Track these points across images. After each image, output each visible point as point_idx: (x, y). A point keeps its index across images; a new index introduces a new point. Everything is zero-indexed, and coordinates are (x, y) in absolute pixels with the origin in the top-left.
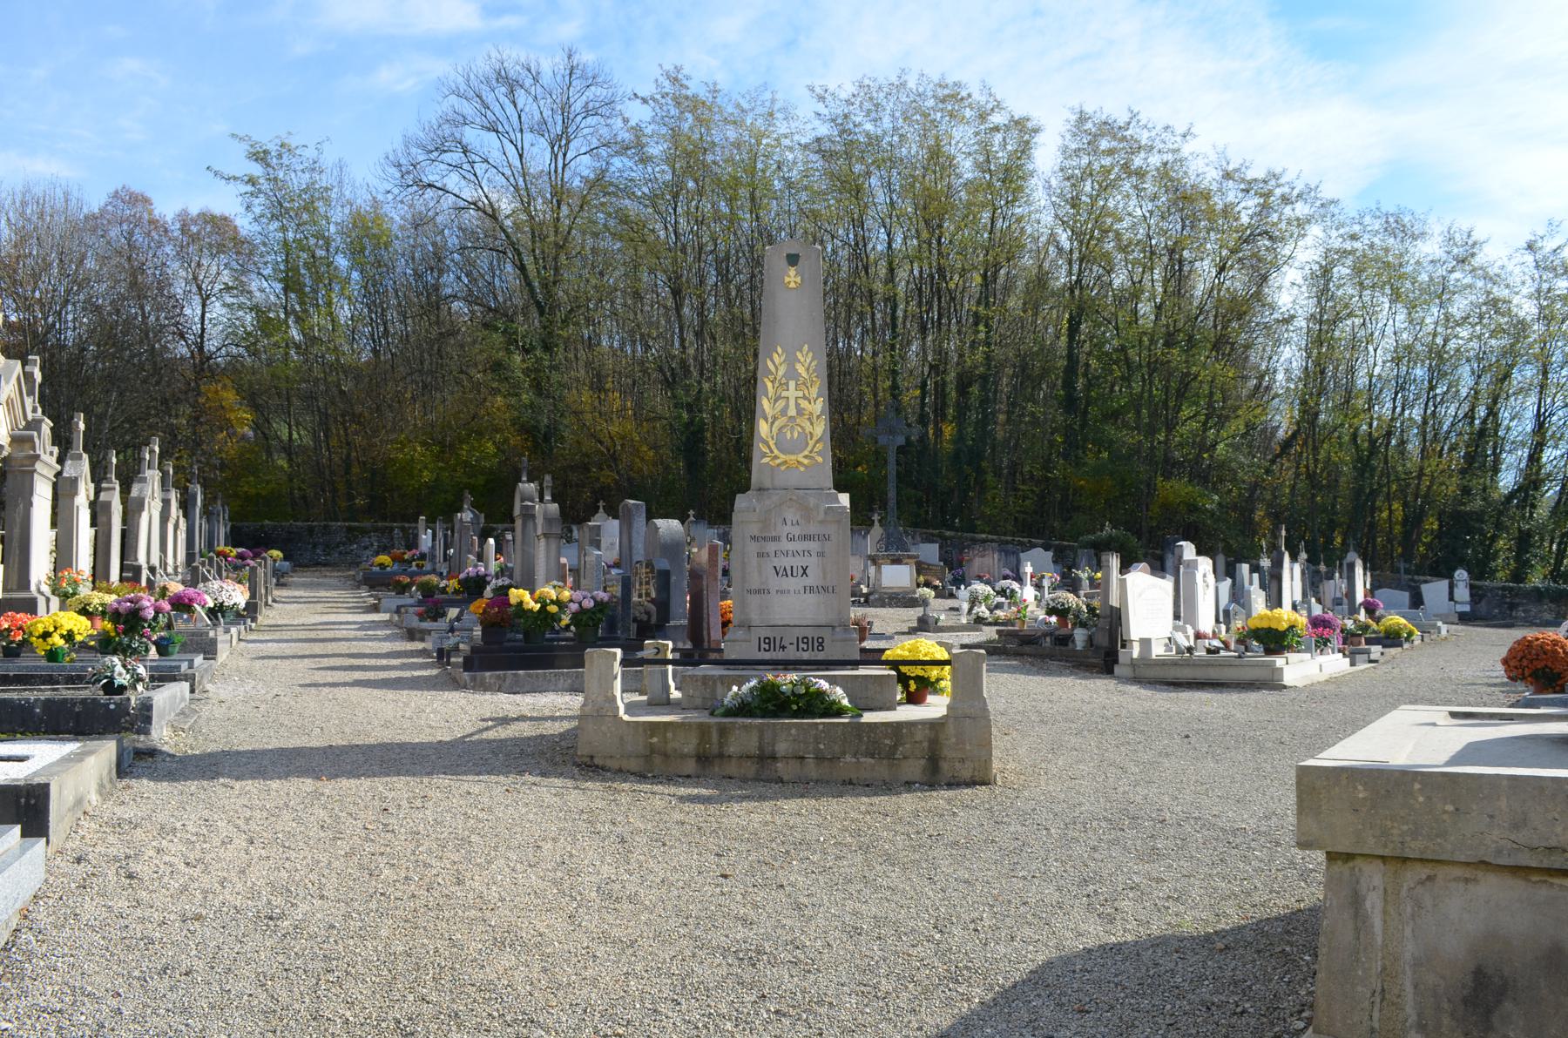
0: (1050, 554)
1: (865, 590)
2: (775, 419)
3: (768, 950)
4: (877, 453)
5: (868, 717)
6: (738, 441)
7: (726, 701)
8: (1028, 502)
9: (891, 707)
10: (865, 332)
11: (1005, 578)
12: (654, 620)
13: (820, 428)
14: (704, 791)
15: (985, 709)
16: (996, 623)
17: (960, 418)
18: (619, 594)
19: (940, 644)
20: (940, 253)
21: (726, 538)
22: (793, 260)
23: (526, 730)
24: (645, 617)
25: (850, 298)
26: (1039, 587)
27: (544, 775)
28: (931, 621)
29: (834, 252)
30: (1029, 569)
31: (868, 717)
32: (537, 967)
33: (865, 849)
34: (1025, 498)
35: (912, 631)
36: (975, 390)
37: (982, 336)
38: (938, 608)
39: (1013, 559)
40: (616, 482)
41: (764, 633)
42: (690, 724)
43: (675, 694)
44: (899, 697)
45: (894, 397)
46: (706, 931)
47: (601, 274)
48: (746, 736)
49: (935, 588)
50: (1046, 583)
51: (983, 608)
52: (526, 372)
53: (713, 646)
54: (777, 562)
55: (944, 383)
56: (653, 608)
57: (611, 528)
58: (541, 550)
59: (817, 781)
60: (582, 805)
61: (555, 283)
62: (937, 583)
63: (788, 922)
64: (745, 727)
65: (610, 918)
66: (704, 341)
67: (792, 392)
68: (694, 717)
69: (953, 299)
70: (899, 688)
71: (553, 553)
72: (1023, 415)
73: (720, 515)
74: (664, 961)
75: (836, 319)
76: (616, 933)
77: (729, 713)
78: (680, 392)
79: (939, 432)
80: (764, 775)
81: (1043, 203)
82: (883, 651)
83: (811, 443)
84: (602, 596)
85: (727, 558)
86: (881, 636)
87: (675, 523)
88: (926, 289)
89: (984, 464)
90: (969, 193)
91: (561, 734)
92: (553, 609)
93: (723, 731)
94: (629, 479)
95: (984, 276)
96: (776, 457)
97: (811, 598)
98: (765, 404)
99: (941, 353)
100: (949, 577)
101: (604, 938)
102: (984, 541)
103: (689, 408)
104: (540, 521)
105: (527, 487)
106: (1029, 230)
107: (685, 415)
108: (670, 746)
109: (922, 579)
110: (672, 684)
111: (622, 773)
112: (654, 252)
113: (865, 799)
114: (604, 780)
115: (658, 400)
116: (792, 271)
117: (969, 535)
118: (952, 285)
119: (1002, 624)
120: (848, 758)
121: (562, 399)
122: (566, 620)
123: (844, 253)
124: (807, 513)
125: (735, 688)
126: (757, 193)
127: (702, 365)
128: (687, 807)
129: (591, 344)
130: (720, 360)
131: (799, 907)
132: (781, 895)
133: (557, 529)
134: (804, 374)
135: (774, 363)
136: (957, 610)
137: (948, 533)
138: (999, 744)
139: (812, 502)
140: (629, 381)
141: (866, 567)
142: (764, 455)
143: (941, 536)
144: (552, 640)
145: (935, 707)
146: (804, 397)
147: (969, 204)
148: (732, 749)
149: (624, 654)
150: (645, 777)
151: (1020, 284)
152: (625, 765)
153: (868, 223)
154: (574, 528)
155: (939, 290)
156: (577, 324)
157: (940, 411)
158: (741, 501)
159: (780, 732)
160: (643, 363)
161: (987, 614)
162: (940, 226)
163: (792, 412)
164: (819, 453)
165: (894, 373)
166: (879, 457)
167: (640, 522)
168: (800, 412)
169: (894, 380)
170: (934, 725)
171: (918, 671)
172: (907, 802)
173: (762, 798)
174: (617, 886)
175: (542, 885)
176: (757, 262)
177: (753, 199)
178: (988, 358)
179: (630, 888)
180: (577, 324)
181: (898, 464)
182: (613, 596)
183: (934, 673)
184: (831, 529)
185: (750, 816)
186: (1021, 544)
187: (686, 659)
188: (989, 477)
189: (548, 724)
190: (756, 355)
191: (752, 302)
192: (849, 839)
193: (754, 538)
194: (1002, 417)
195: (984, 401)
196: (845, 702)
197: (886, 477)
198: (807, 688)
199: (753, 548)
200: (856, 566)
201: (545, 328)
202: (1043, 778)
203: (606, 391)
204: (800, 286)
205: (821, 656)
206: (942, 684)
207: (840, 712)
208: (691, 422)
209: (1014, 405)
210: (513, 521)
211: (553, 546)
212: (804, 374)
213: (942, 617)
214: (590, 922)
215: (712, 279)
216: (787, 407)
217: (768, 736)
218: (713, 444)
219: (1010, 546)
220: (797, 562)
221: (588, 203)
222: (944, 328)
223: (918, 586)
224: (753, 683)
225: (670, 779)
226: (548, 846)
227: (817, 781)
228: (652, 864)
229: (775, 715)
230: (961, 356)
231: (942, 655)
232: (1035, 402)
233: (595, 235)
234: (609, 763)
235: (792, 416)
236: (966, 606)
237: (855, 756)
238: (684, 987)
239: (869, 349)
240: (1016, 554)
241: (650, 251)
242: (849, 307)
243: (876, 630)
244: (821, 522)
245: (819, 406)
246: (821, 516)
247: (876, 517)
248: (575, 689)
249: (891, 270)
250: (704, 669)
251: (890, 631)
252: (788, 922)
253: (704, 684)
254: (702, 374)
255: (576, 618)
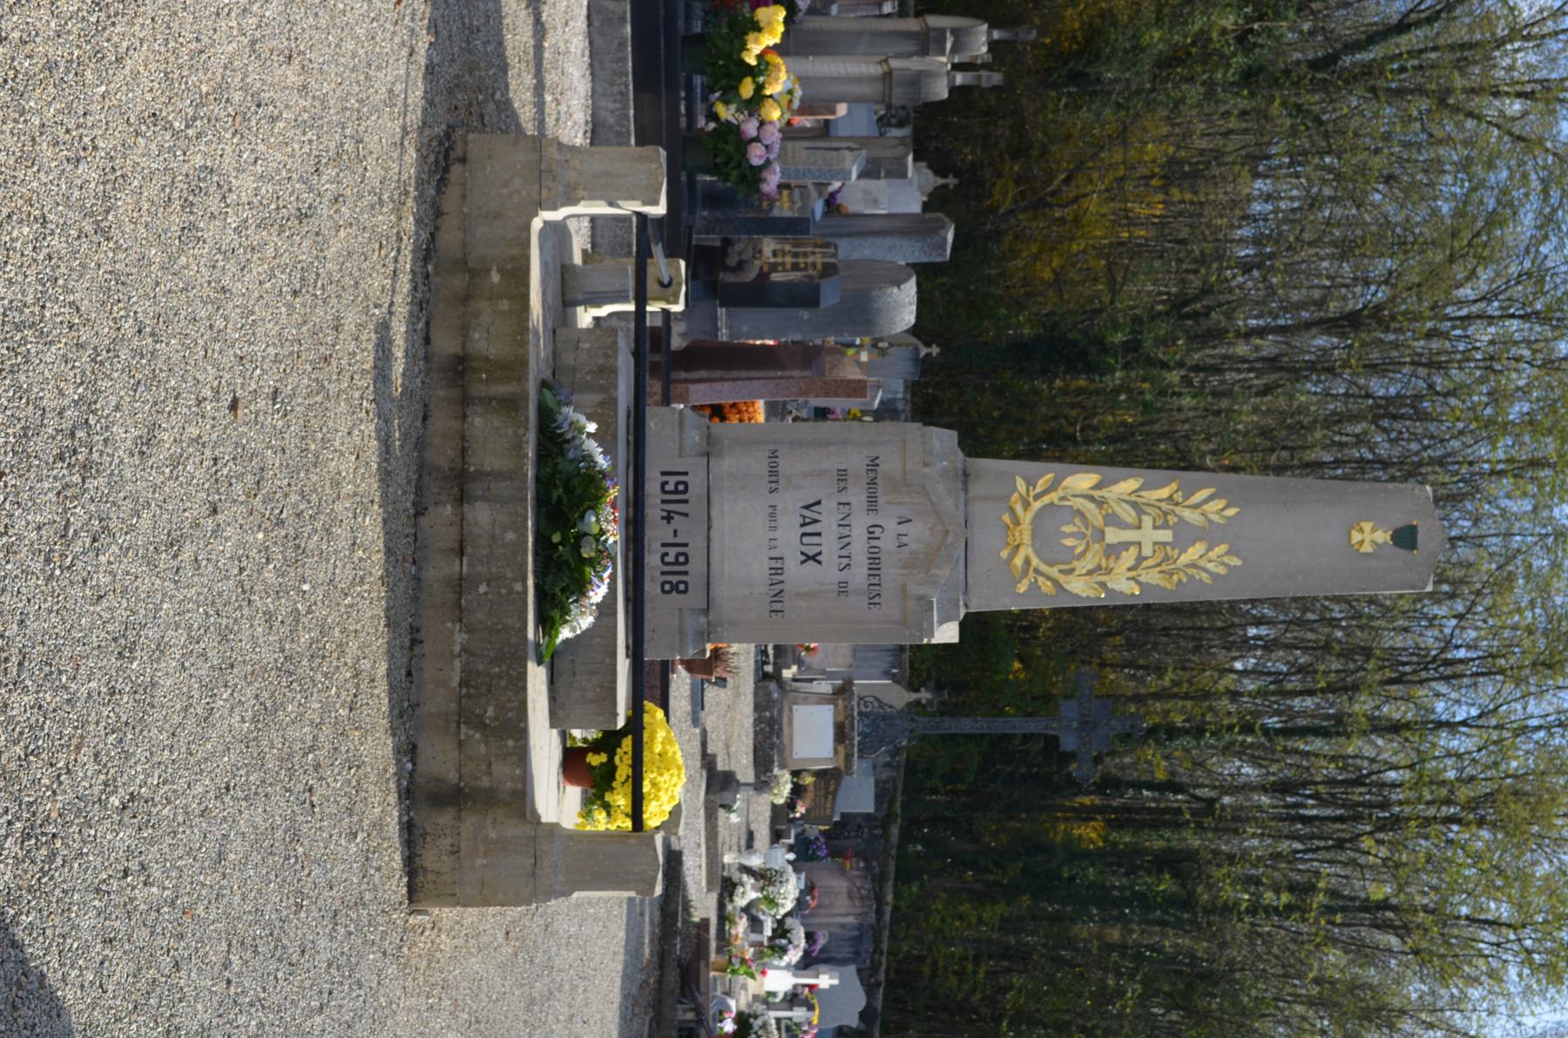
0: (854, 1022)
1: (786, 674)
2: (1100, 503)
3: (91, 484)
4: (1048, 698)
5: (537, 677)
6: (1071, 438)
7: (568, 411)
8: (953, 981)
9: (555, 719)
10: (1279, 677)
11: (810, 937)
12: (726, 277)
13: (1081, 589)
14: (398, 368)
15: (551, 894)
16: (723, 918)
17: (1110, 856)
18: (776, 213)
19: (676, 813)
20: (1428, 822)
21: (886, 412)
22: (1405, 538)
23: (517, 37)
24: (732, 261)
25: (1342, 648)
26: (793, 999)
27: (430, 70)
28: (726, 797)
29: (1432, 620)
30: (825, 981)
31: (537, 677)
32: (57, 52)
33: (287, 667)
34: (960, 974)
35: (708, 761)
36: (1167, 885)
37: (1269, 897)
38: (752, 810)
39: (846, 952)
40: (993, 210)
41: (696, 481)
42: (524, 343)
43: (585, 317)
44: (577, 733)
45: (1153, 731)
46: (128, 370)
47: (1389, 179)
48: (508, 450)
49: (791, 805)
50: (799, 1014)
51: (753, 895)
52: (1203, 37)
53: (677, 389)
54: (829, 506)
55: (1178, 826)
56: (750, 275)
57: (906, 194)
58: (860, 67)
59: (417, 579)
60: (372, 141)
61: (1373, 90)
62: (801, 810)
63: (145, 522)
64: (519, 446)
65: (151, 191)
66: (1260, 373)
67: (1150, 535)
68: (539, 353)
69: (1340, 845)
70: (593, 734)
71: (856, 89)
72: (1119, 975)
73: (927, 403)
74: (67, 290)
75: (1300, 623)
76: (124, 201)
77: (546, 417)
78: (1163, 329)
79: (1085, 814)
80: (427, 487)
81: (1529, 1021)
82: (664, 705)
83: (1054, 571)
84: (772, 180)
85: (849, 416)
86: (698, 702)
87: (908, 317)
88: (1359, 794)
89: (1026, 900)
90: (1546, 878)
91: (508, 103)
92: (747, 89)
93: (512, 405)
94: (997, 235)
95: (1384, 905)
96: (1026, 505)
97: (760, 570)
98: (1128, 485)
99: (1234, 823)
100: (814, 831)
101: (113, 180)
102: (879, 898)
103: (1133, 346)
104: (915, 64)
105: (980, 40)
106: (1475, 993)
107: (1119, 337)
108: (484, 305)
109: (808, 780)
110: (605, 311)
111: (433, 216)
112: (1433, 274)
113: (382, 668)
114: (420, 183)
115: (1146, 289)
116: (1383, 537)
117: (892, 869)
118: (1367, 843)
119: (721, 931)
120: (460, 638)
121: (1150, 105)
122: (726, 112)
123: (1430, 640)
124: (922, 563)
125: (592, 427)
126: (1545, 473)
127: (1216, 370)
128: (369, 337)
129: (1254, 160)
130: (1224, 403)
131: (174, 543)
132: (197, 509)
133: (899, 96)
134: (1184, 559)
135: (1206, 502)
136: (750, 844)
137: (895, 830)
138: (489, 920)
139: (943, 573)
140: (1184, 233)
141: (830, 676)
142: (1031, 483)
143: (888, 818)
144: (690, 88)
145: (557, 802)
146: (1140, 559)
147: (1524, 878)
148: (478, 422)
149: (659, 221)
150: (426, 260)
151: (1371, 974)
152: (450, 224)
153: (1488, 687)
154: (906, 132)
155: (1357, 818)
156: (1294, 132)
157: (1125, 818)
158: (943, 440)
159: (509, 512)
160: (1220, 257)
161: (741, 902)
162: (1481, 822)
163: (1113, 536)
164: (1034, 587)
165: (1199, 732)
166: (1041, 702)
167: (908, 252)
168: (1114, 551)
169: (1186, 732)
170: (520, 799)
171: (623, 770)
172: (377, 748)
173: (386, 476)
174: (214, 204)
175: (216, 64)
176: (1411, 471)
177: (1535, 464)
178: (1229, 909)
179: (210, 231)
180: (1294, 132)
181: (1027, 738)
182: (772, 202)
183: (620, 799)
184: (890, 608)
185: (350, 454)
186: (874, 968)
187: (649, 341)
188: (1001, 909)
189: (529, 80)
190: (1234, 469)
191: (1338, 463)
192: (305, 638)
193: (874, 464)
194: (1115, 934)
195: (1145, 902)
196: (565, 633)
197: (1002, 713)
198: (591, 562)
199: (856, 461)
200: (832, 655)
201: (1287, 72)
202: (422, 1003)
203: (1164, 189)
204: (1354, 552)
205: (651, 588)
206: (600, 816)
207: (547, 623)
208: (1105, 349)
209: (1139, 958)
210: (918, 14)
211: (867, 90)
212: (1184, 559)
213: (734, 818)
214: (145, 153)
215: (1379, 387)
216: (1124, 526)
217: (503, 488)
218: (1065, 392)
219: (868, 946)
220: (829, 546)
221: (1528, 150)
222: (1285, 827)
223: (796, 774)
224: (602, 462)
225: (422, 305)
226: (292, 75)
227: (417, 579)
228: (258, 269)
229: (542, 501)
230: (1231, 858)
231: (654, 814)
232: (1144, 998)
233: (1465, 165)
234: (452, 192)
235: (1106, 534)
236: (755, 861)
237: (465, 650)
238: (18, 327)
239: (1250, 685)
240: (855, 958)
241: (1433, 274)
242: (1327, 647)
243: (711, 693)
244: (904, 590)
245: (1124, 585)
246: (914, 590)
247: (925, 695)
248: (597, 131)
249: (1395, 728)
250: (625, 363)
251: (710, 719)
252: (145, 522)
253: (601, 370)
254: (1196, 368)
255: (729, 131)
